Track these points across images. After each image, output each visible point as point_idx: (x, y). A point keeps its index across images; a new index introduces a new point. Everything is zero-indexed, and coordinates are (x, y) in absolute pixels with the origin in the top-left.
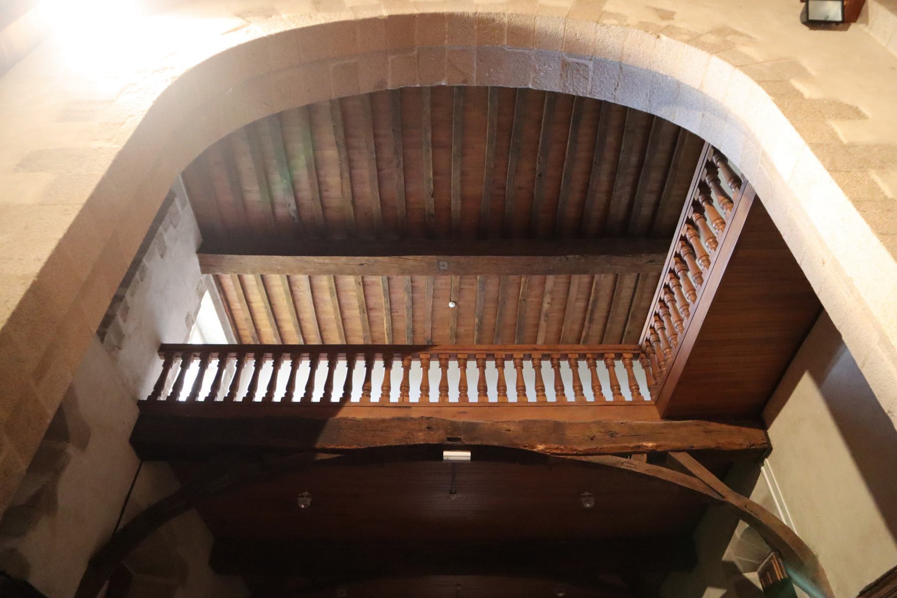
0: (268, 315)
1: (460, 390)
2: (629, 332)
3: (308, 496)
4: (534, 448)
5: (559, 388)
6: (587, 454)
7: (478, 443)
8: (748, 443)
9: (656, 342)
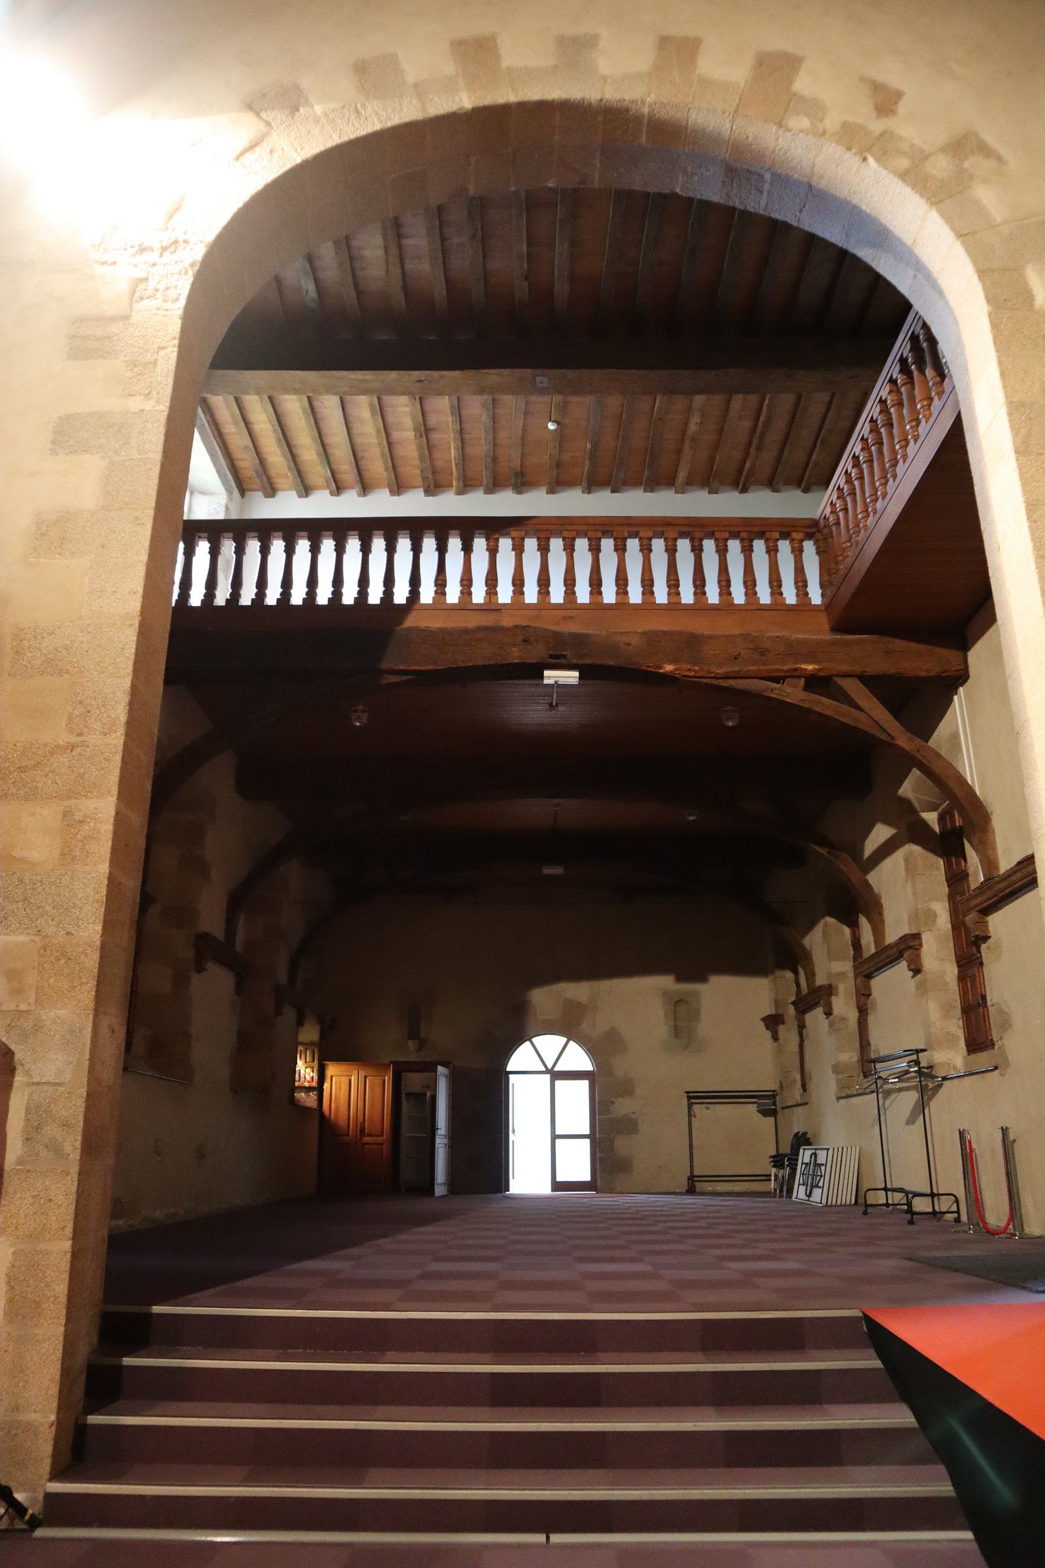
0: (279, 442)
1: (565, 585)
2: (816, 464)
3: (363, 711)
4: (660, 668)
5: (698, 583)
6: (727, 677)
7: (588, 661)
8: (937, 669)
9: (844, 512)
